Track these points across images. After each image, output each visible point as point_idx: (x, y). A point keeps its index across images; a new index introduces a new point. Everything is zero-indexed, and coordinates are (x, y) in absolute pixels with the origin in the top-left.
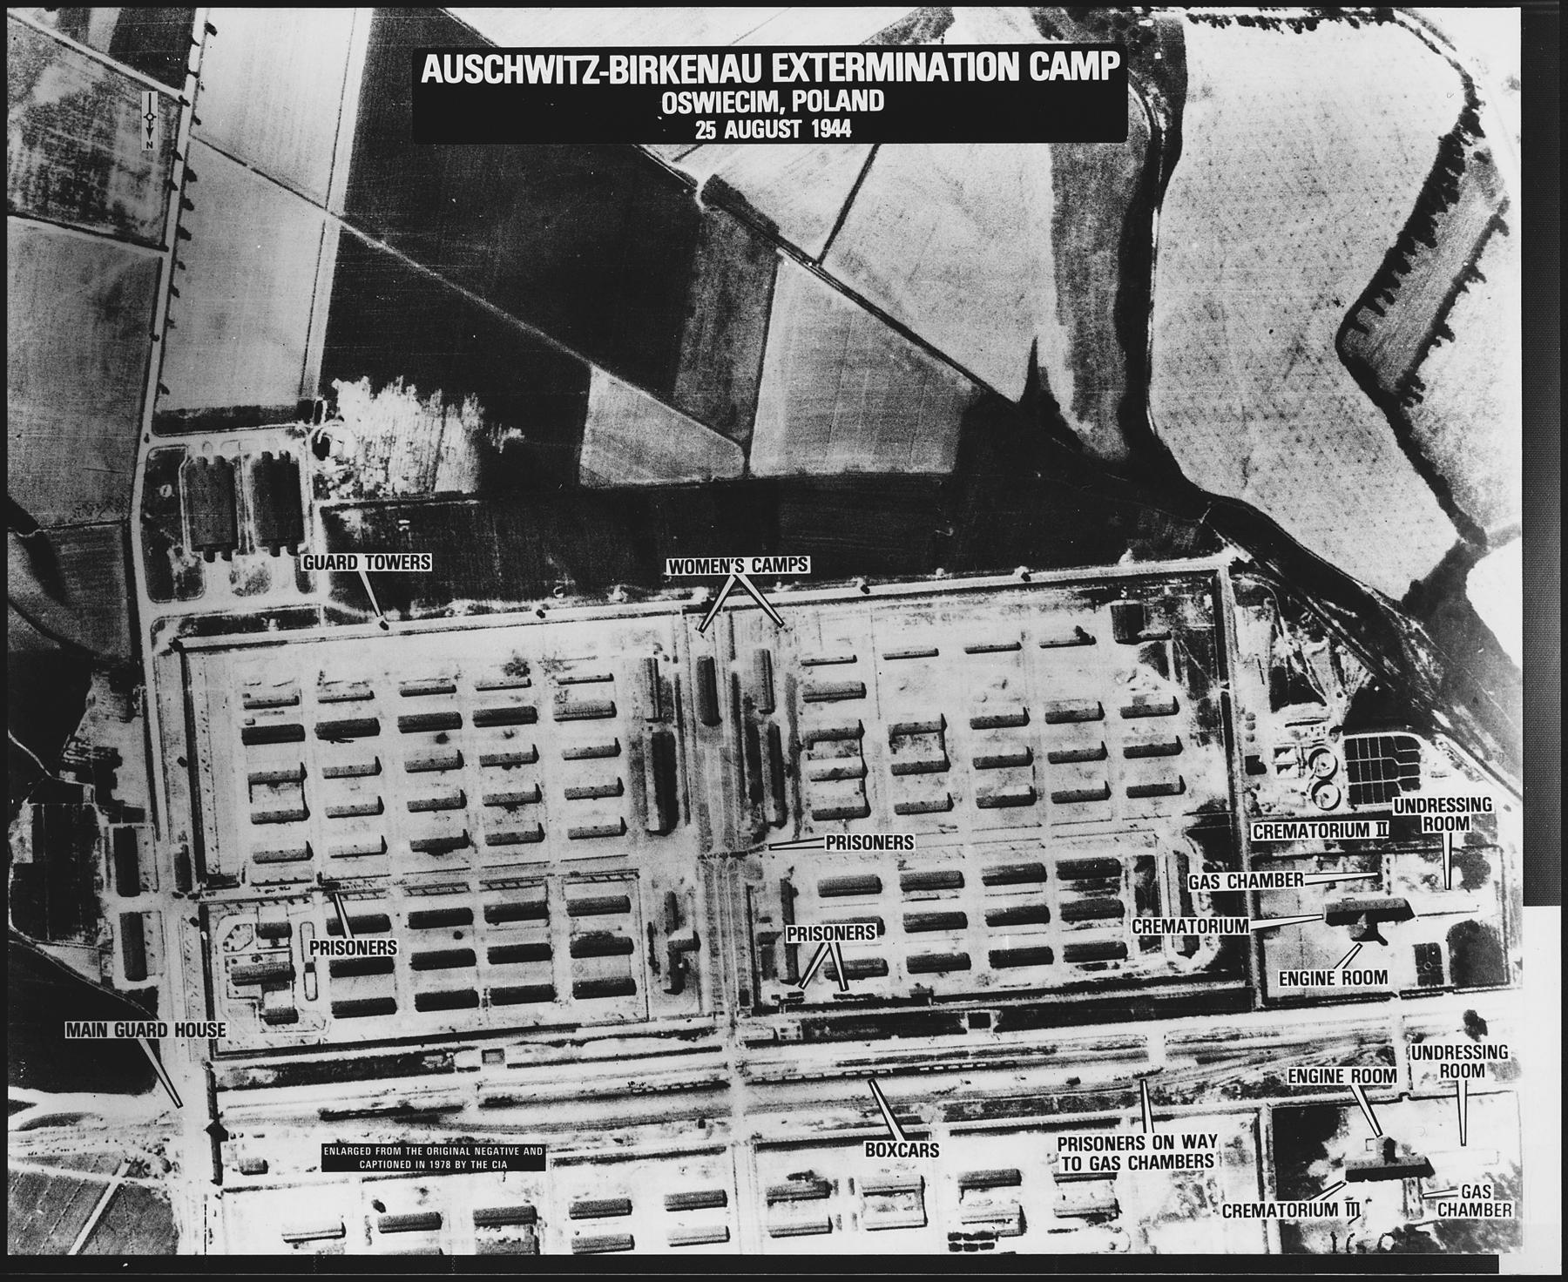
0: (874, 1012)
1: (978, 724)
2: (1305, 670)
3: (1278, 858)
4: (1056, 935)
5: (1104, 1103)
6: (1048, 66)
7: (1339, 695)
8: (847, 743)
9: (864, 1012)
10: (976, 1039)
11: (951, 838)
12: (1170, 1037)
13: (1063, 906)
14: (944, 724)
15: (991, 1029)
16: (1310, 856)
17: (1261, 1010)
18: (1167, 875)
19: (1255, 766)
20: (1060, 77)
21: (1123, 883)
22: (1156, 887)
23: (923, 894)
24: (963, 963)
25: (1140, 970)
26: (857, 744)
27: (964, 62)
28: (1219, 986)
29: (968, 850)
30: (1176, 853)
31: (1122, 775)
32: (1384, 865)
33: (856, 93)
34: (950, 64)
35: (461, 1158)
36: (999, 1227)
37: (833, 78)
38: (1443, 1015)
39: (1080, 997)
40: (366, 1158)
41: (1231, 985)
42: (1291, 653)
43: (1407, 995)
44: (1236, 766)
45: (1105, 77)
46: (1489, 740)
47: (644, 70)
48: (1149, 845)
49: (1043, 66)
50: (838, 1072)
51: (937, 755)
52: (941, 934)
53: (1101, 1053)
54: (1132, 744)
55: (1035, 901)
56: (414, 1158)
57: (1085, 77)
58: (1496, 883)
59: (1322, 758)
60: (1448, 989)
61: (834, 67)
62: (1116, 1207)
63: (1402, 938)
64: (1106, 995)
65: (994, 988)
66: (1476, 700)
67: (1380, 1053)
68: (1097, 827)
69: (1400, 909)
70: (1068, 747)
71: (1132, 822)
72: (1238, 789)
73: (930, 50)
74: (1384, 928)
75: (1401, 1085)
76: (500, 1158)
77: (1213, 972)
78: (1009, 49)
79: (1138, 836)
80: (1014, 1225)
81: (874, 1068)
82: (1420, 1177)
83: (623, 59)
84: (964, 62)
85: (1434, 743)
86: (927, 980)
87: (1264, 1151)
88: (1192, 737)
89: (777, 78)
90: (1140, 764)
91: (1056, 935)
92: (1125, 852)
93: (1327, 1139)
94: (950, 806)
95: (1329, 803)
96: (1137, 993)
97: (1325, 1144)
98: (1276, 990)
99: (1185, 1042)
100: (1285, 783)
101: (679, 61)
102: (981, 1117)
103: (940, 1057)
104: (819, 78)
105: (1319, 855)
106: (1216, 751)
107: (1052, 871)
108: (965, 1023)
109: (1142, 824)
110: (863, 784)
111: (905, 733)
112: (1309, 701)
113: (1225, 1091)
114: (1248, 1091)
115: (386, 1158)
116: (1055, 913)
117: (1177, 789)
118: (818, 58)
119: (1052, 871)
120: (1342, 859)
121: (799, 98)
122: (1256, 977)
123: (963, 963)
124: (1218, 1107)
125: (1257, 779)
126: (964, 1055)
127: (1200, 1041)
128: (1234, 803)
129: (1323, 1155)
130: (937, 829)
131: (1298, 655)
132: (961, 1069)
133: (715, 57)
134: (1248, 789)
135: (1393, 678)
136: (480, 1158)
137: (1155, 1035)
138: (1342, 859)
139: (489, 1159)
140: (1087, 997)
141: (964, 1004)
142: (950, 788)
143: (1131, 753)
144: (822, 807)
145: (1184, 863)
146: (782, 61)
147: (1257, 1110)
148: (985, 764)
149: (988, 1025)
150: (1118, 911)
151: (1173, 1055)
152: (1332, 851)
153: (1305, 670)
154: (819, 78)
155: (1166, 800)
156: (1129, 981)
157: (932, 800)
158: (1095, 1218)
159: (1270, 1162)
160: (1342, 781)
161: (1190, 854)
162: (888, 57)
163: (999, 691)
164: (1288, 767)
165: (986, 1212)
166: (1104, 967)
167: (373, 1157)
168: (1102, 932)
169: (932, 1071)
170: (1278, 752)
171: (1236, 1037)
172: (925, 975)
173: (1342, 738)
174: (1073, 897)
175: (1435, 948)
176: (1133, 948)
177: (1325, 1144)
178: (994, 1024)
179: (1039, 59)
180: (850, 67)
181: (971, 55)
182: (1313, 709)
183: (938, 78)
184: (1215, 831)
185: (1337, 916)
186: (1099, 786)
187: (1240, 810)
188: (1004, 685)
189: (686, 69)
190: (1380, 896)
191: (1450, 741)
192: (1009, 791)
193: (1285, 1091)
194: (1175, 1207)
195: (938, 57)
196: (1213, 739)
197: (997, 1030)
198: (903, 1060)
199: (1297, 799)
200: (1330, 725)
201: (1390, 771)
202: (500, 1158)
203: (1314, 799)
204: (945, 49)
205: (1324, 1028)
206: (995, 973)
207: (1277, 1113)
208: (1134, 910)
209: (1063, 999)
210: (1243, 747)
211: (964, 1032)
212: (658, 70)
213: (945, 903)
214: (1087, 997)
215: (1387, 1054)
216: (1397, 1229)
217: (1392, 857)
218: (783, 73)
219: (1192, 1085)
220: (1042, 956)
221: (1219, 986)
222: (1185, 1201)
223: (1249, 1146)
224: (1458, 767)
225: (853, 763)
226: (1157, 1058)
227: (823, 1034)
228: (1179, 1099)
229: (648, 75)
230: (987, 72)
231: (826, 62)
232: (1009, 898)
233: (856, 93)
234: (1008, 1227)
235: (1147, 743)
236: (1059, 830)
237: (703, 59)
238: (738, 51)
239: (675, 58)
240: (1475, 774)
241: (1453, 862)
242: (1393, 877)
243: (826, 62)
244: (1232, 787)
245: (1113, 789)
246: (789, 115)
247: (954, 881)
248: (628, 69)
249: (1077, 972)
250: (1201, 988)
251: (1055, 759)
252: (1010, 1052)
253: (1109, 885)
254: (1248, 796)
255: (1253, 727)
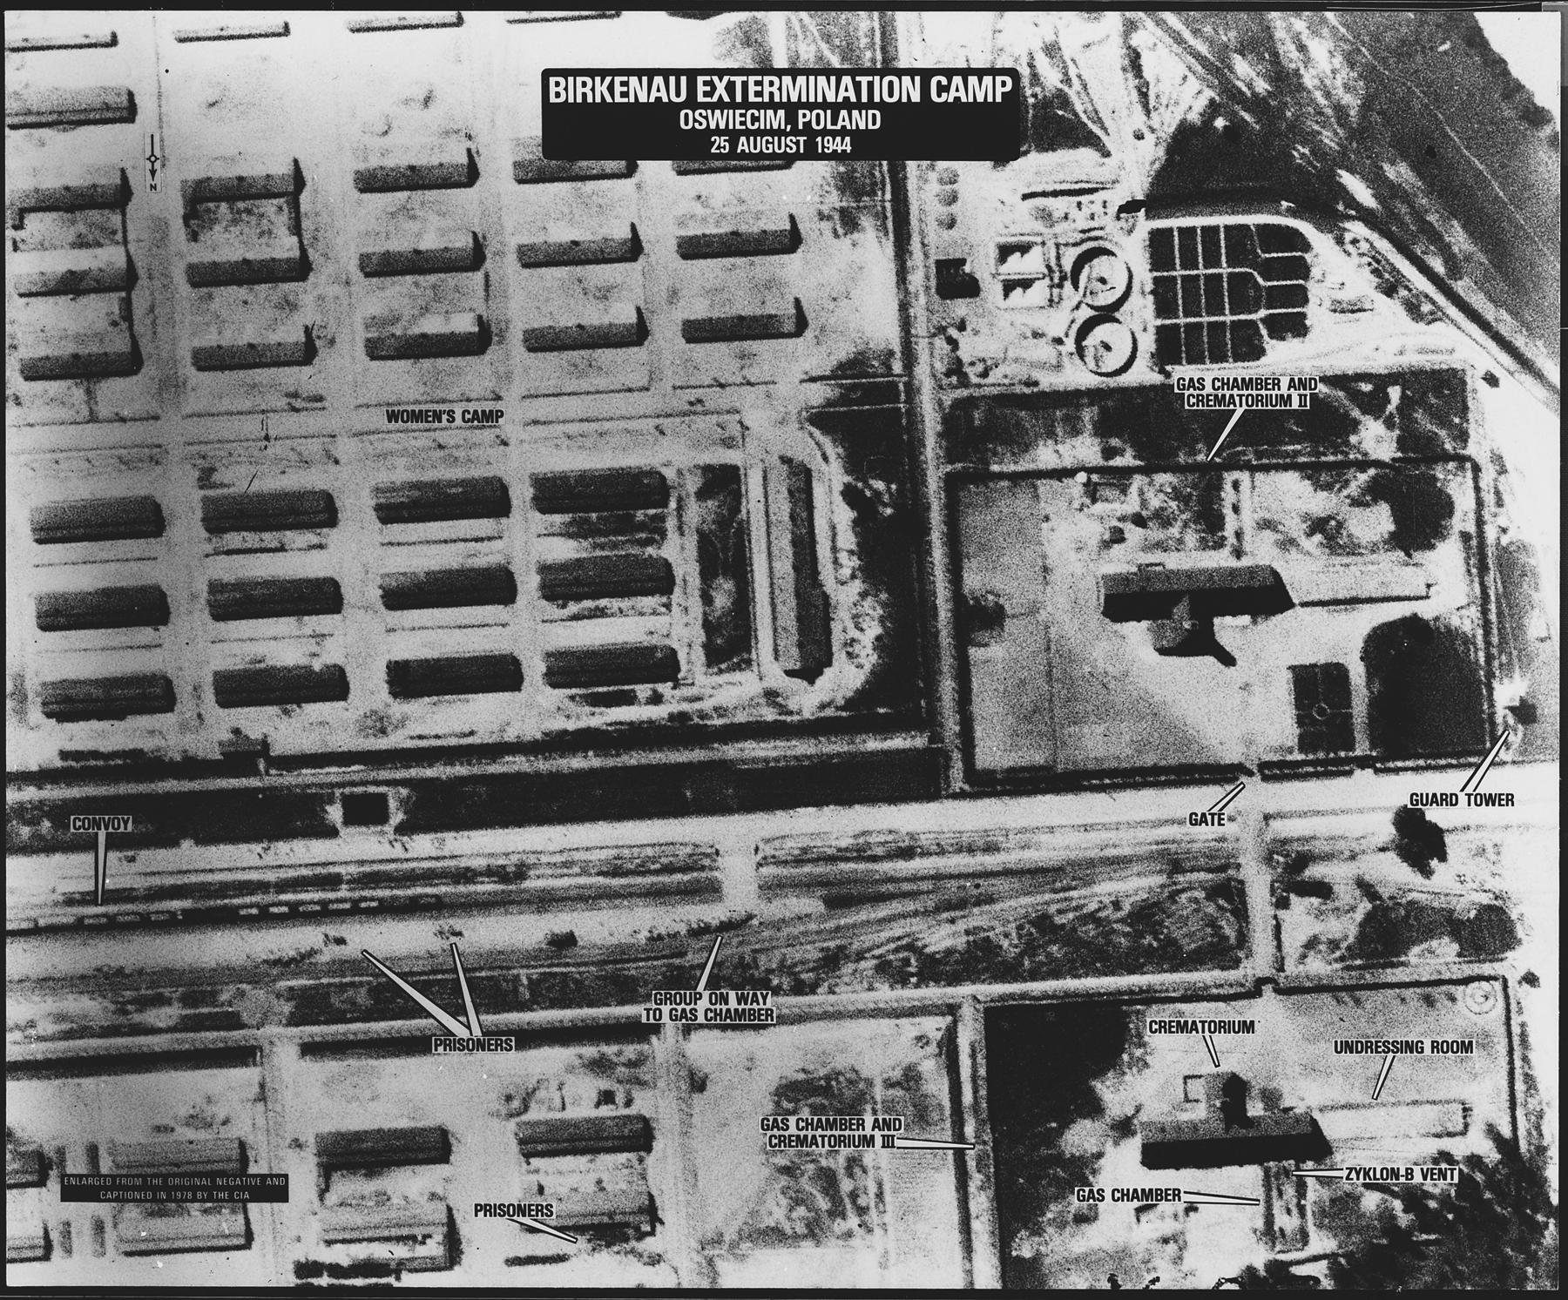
0: (143, 788)
1: (371, 182)
2: (1067, 80)
3: (1001, 476)
4: (530, 630)
5: (627, 990)
6: (947, 89)
7: (1139, 136)
8: (94, 215)
9: (123, 789)
10: (360, 846)
11: (310, 422)
12: (768, 850)
13: (544, 569)
14: (298, 177)
15: (389, 828)
16: (1069, 473)
17: (962, 795)
18: (764, 504)
19: (955, 280)
20: (957, 99)
21: (671, 524)
22: (743, 532)
23: (252, 539)
24: (332, 685)
25: (706, 705)
26: (116, 219)
27: (870, 84)
28: (873, 744)
29: (346, 448)
30: (785, 460)
31: (674, 295)
32: (1228, 494)
34: (857, 86)
36: (401, 1252)
37: (752, 98)
38: (1355, 809)
39: (577, 763)
41: (898, 742)
42: (1036, 46)
43: (1276, 771)
44: (916, 279)
45: (999, 99)
46: (1459, 239)
47: (580, 90)
48: (728, 443)
49: (942, 89)
50: (67, 916)
51: (285, 247)
52: (285, 625)
53: (622, 881)
54: (694, 230)
55: (487, 556)
57: (980, 99)
58: (1465, 537)
59: (1100, 266)
60: (1364, 762)
61: (752, 89)
62: (651, 1212)
63: (1270, 650)
64: (633, 759)
65: (397, 740)
66: (1431, 151)
67: (1213, 892)
68: (619, 404)
69: (1263, 589)
70: (561, 234)
71: (692, 395)
72: (920, 328)
73: (839, 74)
74: (1228, 629)
75: (1258, 963)
77: (859, 713)
79: (704, 424)
80: (434, 1248)
81: (141, 907)
82: (1300, 1160)
83: (561, 80)
84: (870, 84)
85: (1340, 241)
86: (258, 721)
87: (967, 1097)
88: (822, 216)
89: (701, 98)
90: (709, 269)
91: (530, 630)
92: (676, 456)
93: (1100, 1073)
94: (307, 353)
95: (1112, 362)
96: (698, 755)
97: (1098, 1085)
98: (992, 752)
99: (798, 862)
100: (1020, 318)
101: (612, 82)
102: (367, 1017)
103: (282, 886)
104: (739, 99)
105: (1090, 470)
106: (872, 250)
107: (522, 493)
108: (335, 813)
109: (714, 398)
110: (127, 305)
111: (218, 199)
112: (1075, 145)
113: (883, 968)
114: (935, 969)
116: (528, 583)
117: (789, 326)
118: (739, 80)
119: (522, 493)
120: (1138, 481)
122: (952, 725)
123: (332, 685)
124: (865, 999)
125: (960, 308)
126: (333, 881)
127: (831, 859)
128: (910, 359)
129: (1094, 1108)
130: (282, 403)
131: (1052, 50)
132: (324, 913)
133: (645, 79)
134: (941, 330)
135: (1256, 104)
137: (738, 843)
138: (1138, 481)
140: (591, 761)
141: (333, 773)
142: (308, 314)
143: (692, 249)
144: (42, 351)
145: (801, 480)
146: (705, 83)
147: (952, 1009)
148: (382, 267)
149: (383, 818)
150: (660, 581)
151: (771, 889)
152: (1118, 462)
153: (1067, 80)
154: (739, 99)
155: (763, 348)
156: (683, 730)
157: (273, 338)
158: (609, 1231)
159: (980, 1123)
160: (1141, 313)
161: (816, 463)
163: (416, 111)
164: (1026, 284)
165: (376, 1219)
166: (629, 699)
168: (623, 626)
169: (265, 918)
170: (1005, 252)
171: (907, 853)
172: (252, 711)
173: (1145, 225)
174: (565, 550)
175: (1335, 674)
176: (692, 660)
177: (1098, 1085)
178: (397, 817)
179: (939, 82)
180: (767, 89)
181: (877, 78)
182: (1075, 163)
184: (864, 412)
185: (1127, 600)
186: (622, 314)
187: (922, 372)
188: (427, 101)
189: (618, 89)
190: (1220, 559)
191: (1374, 237)
192: (432, 325)
193: (1009, 972)
194: (776, 1212)
195: (847, 80)
196: (867, 222)
197: (402, 829)
198: (204, 890)
199: (1045, 351)
200: (1117, 197)
201: (1243, 294)
203: (1080, 351)
205: (1095, 837)
206: (398, 708)
207: (996, 1017)
208: (695, 582)
209: (542, 765)
210: (932, 239)
211: (332, 833)
212: (593, 89)
213: (297, 559)
214: (591, 761)
215: (1231, 893)
216: (1250, 1270)
217: (1244, 477)
218: (706, 94)
219: (812, 953)
220: (499, 674)
221: (873, 744)
222: (797, 1202)
223: (937, 1086)
224: (1389, 290)
225: (108, 257)
226: (740, 889)
227: (36, 836)
228: (786, 982)
229: (584, 95)
230: (891, 95)
231: (745, 85)
232: (434, 548)
234: (421, 1251)
235: (725, 228)
236: (542, 409)
237: (634, 80)
238: (666, 73)
239: (608, 79)
240: (1426, 308)
241: (1374, 493)
242: (1248, 519)
243: (745, 85)
244: (906, 324)
245: (656, 324)
247: (318, 512)
248: (566, 89)
249: (572, 707)
250: (835, 746)
251: (532, 258)
252: (429, 876)
253: (642, 526)
254: (940, 342)
255: (953, 199)
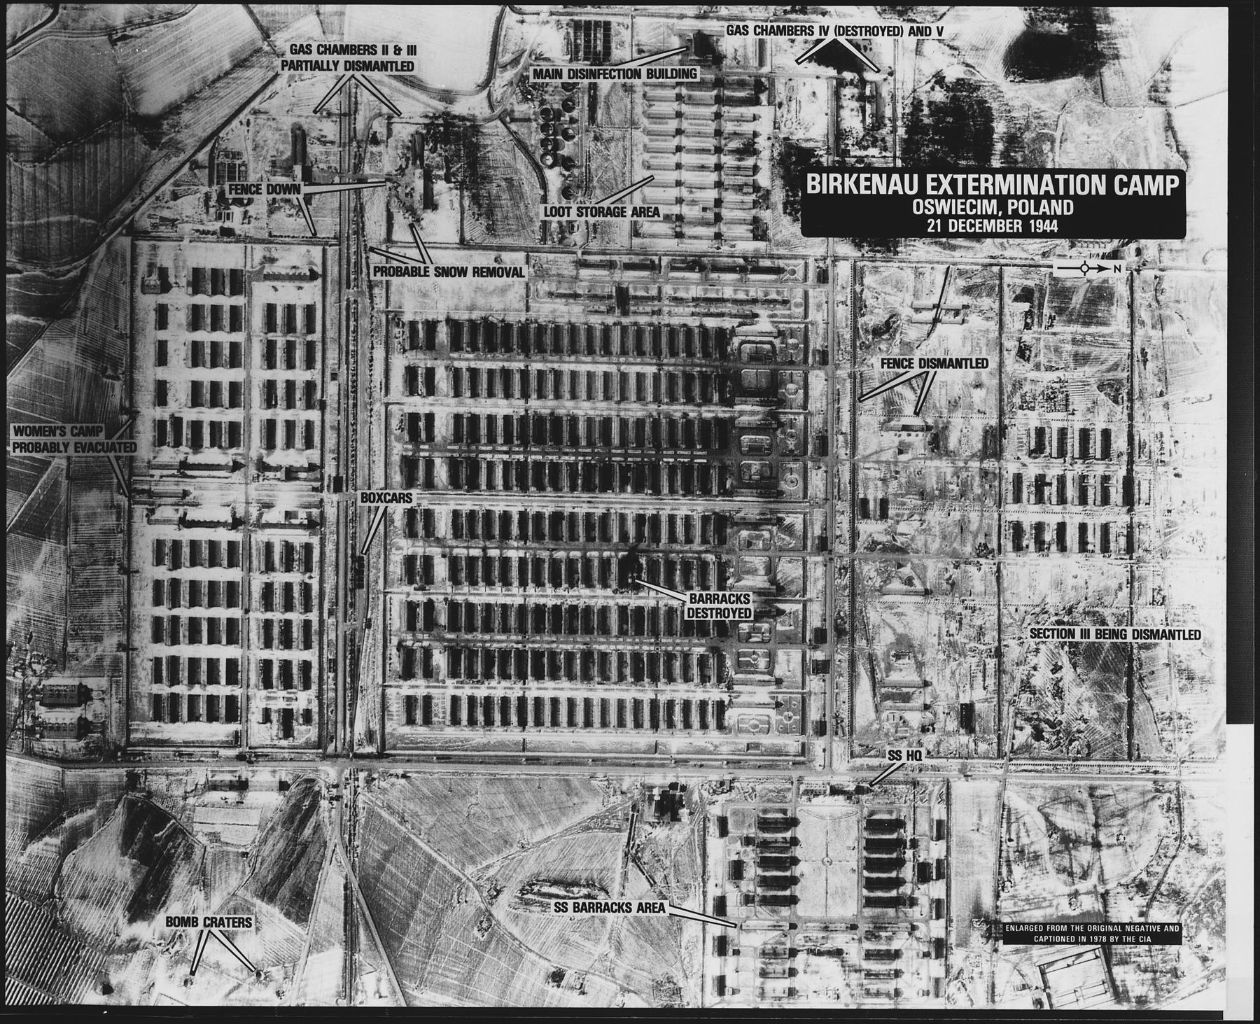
6: (1127, 185)
20: (1136, 193)
27: (1066, 182)
33: (1053, 202)
35: (1114, 933)
40: (1039, 934)
47: (832, 184)
49: (1123, 185)
56: (1077, 934)
57: (1154, 193)
61: (971, 184)
76: (1145, 934)
78: (1099, 172)
84: (1066, 182)
115: (1055, 933)
121: (1011, 205)
136: (1130, 934)
139: (1137, 935)
162: (1010, 177)
167: (1045, 933)
180: (983, 185)
183: (895, 192)
189: (863, 183)
202: (1145, 934)
204: (1053, 172)
218: (933, 188)
230: (1083, 189)
231: (965, 181)
233: (1053, 202)
246: (1005, 217)
